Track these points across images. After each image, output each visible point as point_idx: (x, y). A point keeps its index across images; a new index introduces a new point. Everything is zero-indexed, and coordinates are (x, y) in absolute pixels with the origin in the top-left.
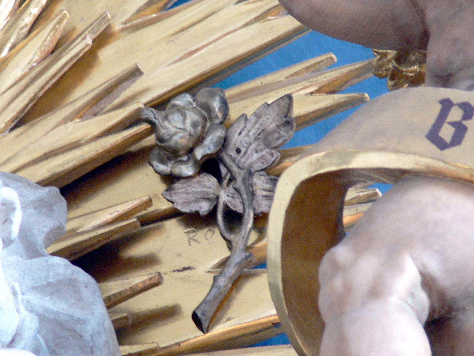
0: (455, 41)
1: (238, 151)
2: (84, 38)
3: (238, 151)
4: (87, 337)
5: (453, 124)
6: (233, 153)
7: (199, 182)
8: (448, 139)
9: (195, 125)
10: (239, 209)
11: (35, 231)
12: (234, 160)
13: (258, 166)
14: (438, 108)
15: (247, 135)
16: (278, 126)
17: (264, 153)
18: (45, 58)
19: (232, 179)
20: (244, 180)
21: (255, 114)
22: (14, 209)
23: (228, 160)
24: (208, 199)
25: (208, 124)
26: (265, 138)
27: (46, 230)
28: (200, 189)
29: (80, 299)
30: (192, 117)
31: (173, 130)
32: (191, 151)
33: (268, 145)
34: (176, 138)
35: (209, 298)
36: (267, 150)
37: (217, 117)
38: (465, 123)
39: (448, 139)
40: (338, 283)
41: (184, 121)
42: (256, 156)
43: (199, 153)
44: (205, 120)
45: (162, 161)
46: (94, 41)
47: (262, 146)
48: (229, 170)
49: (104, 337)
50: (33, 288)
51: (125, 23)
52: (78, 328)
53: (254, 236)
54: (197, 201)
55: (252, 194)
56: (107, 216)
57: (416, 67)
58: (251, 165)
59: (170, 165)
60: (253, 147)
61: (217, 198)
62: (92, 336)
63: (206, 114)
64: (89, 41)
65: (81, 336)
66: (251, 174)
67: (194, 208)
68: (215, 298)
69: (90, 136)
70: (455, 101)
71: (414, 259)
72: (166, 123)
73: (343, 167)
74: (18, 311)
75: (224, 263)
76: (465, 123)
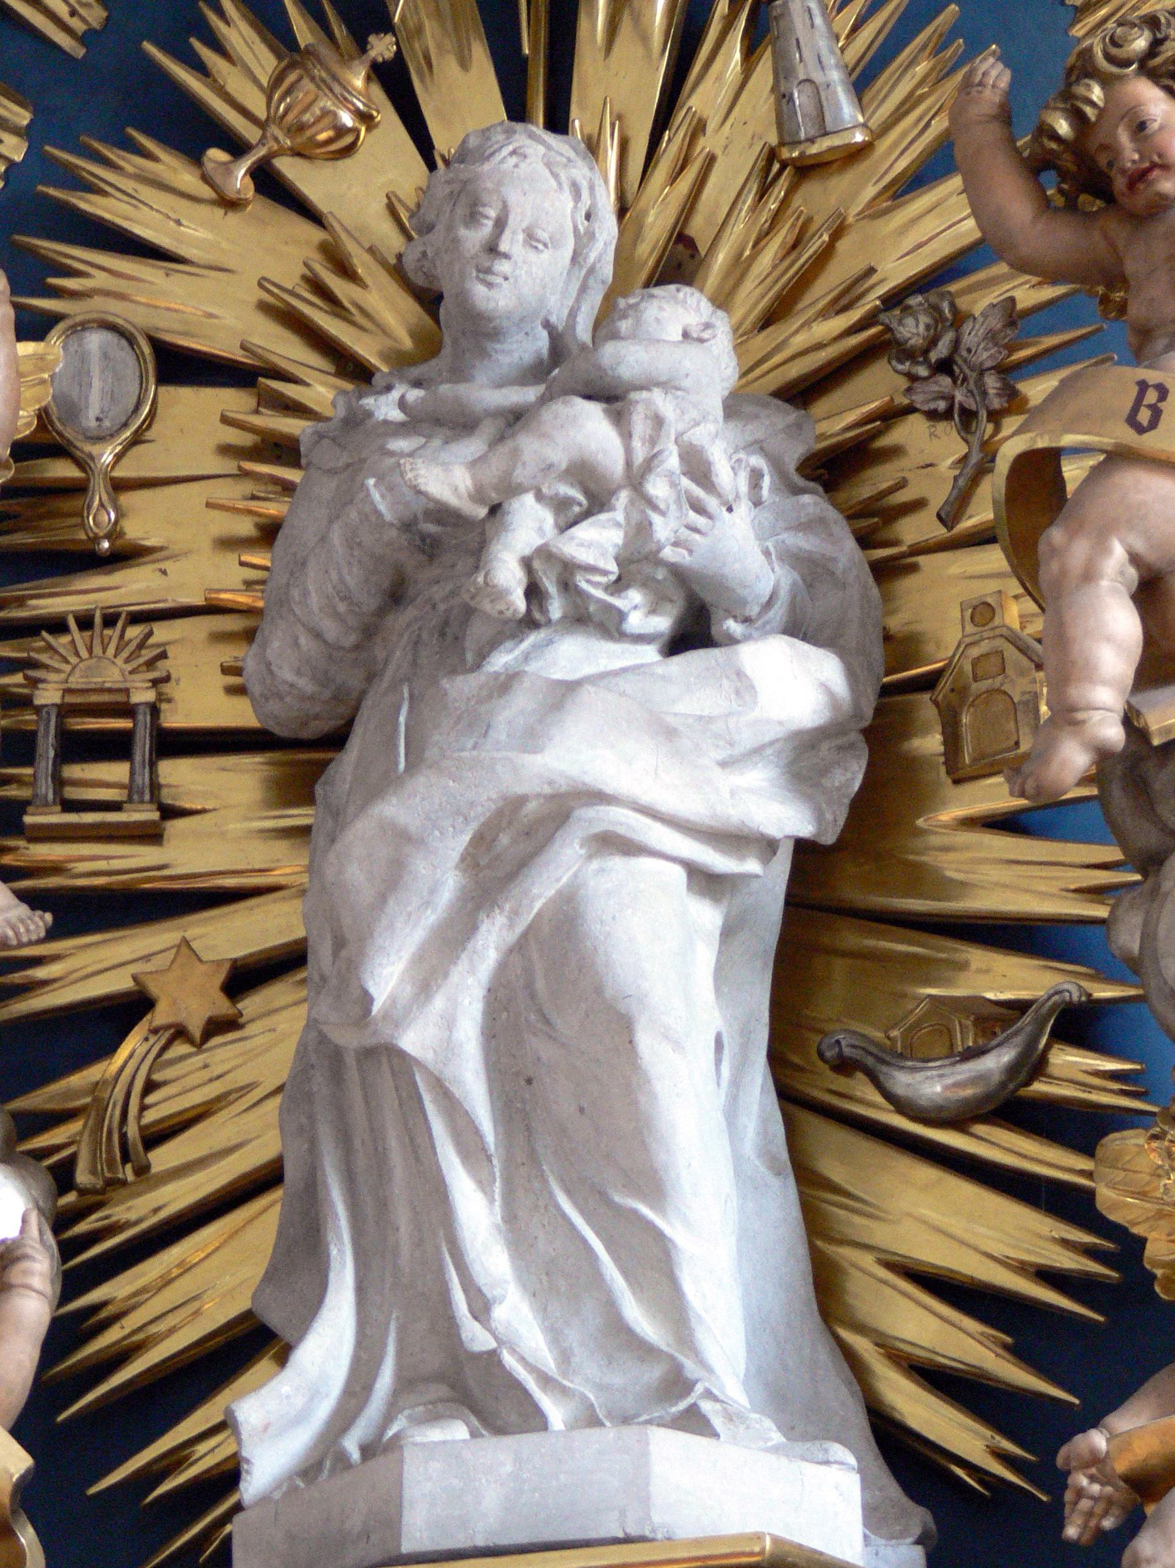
0: (1152, 300)
1: (969, 351)
2: (822, 235)
3: (969, 351)
4: (839, 572)
5: (1149, 406)
6: (964, 353)
7: (935, 383)
8: (1145, 423)
9: (928, 327)
10: (974, 407)
11: (786, 459)
12: (965, 361)
13: (989, 364)
14: (1135, 390)
15: (976, 335)
16: (1004, 326)
17: (992, 351)
18: (788, 253)
19: (965, 380)
20: (976, 383)
21: (982, 314)
22: (763, 476)
23: (960, 361)
24: (943, 398)
25: (940, 326)
26: (993, 338)
27: (796, 456)
28: (937, 388)
29: (831, 535)
30: (924, 319)
31: (908, 335)
32: (926, 352)
33: (996, 344)
34: (912, 342)
35: (952, 499)
36: (996, 349)
37: (947, 319)
38: (1159, 405)
39: (1145, 423)
40: (1054, 566)
41: (917, 326)
42: (985, 355)
43: (934, 356)
44: (936, 321)
45: (901, 362)
46: (830, 237)
47: (990, 345)
48: (961, 371)
49: (854, 572)
50: (786, 529)
51: (858, 215)
52: (830, 566)
53: (990, 428)
54: (935, 399)
55: (984, 393)
56: (852, 417)
57: (1122, 294)
58: (981, 364)
59: (908, 364)
60: (982, 346)
61: (953, 398)
62: (843, 573)
63: (937, 315)
64: (826, 237)
65: (833, 573)
66: (982, 373)
67: (932, 406)
68: (957, 499)
69: (835, 333)
70: (1151, 383)
71: (1122, 541)
72: (901, 328)
73: (1054, 445)
74: (773, 570)
75: (965, 458)
76: (1159, 405)
